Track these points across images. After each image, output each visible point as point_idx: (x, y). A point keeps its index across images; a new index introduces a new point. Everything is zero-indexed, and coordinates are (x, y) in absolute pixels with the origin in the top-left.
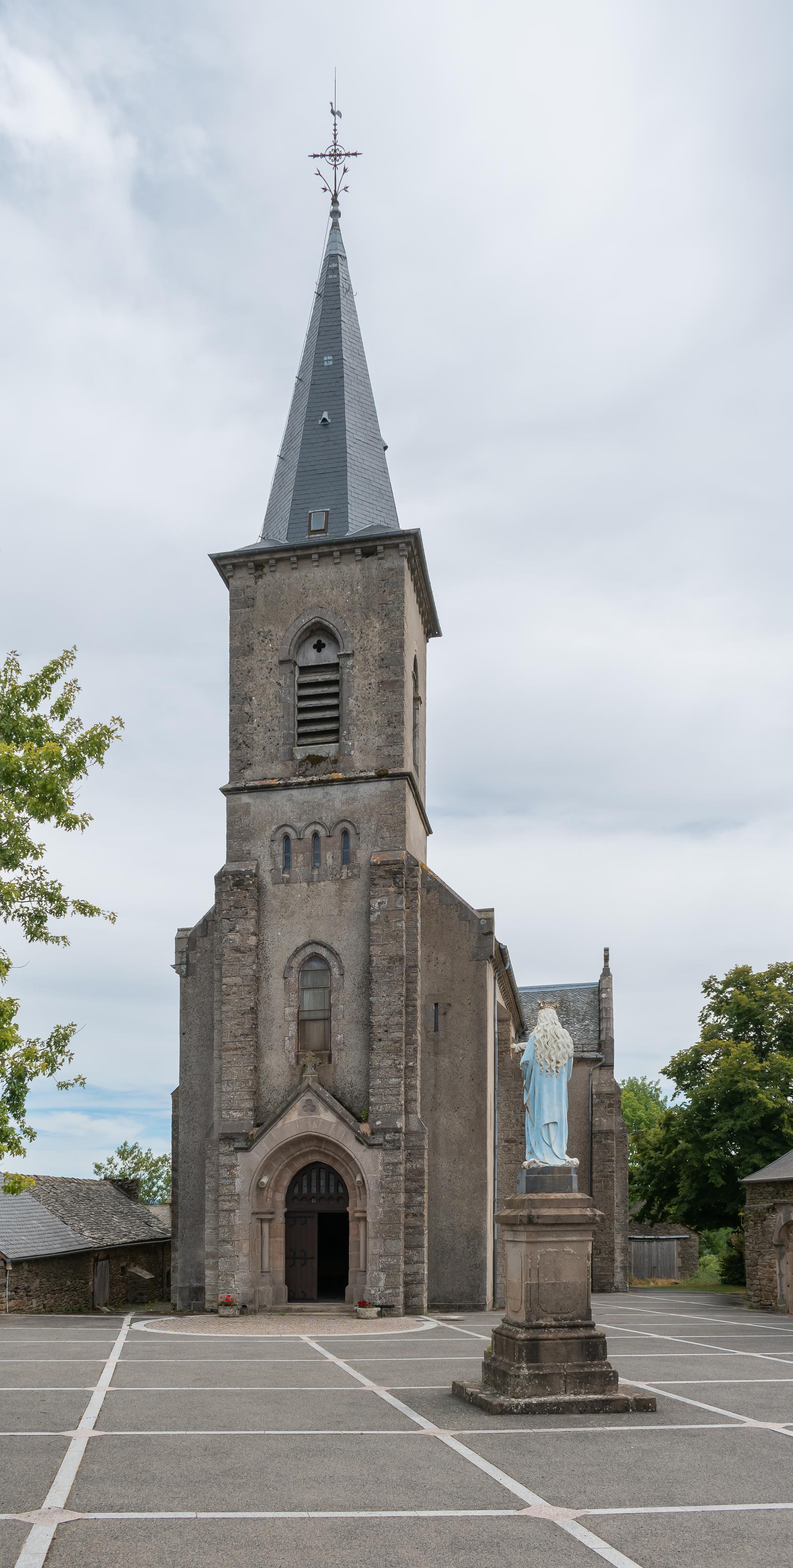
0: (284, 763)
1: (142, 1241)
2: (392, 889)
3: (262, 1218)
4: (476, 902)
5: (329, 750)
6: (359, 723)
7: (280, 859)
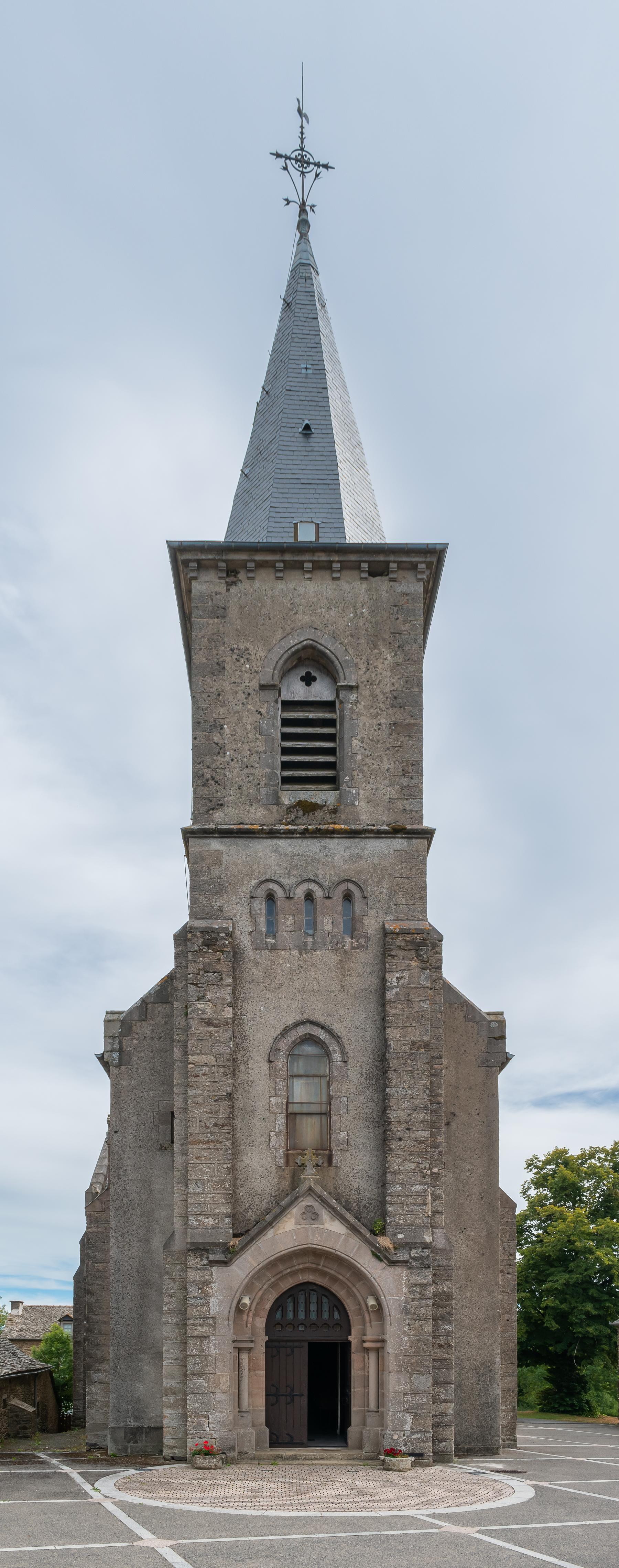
0: (266, 806)
1: (19, 1372)
4: (484, 1004)
5: (324, 796)
6: (365, 768)
7: (262, 920)
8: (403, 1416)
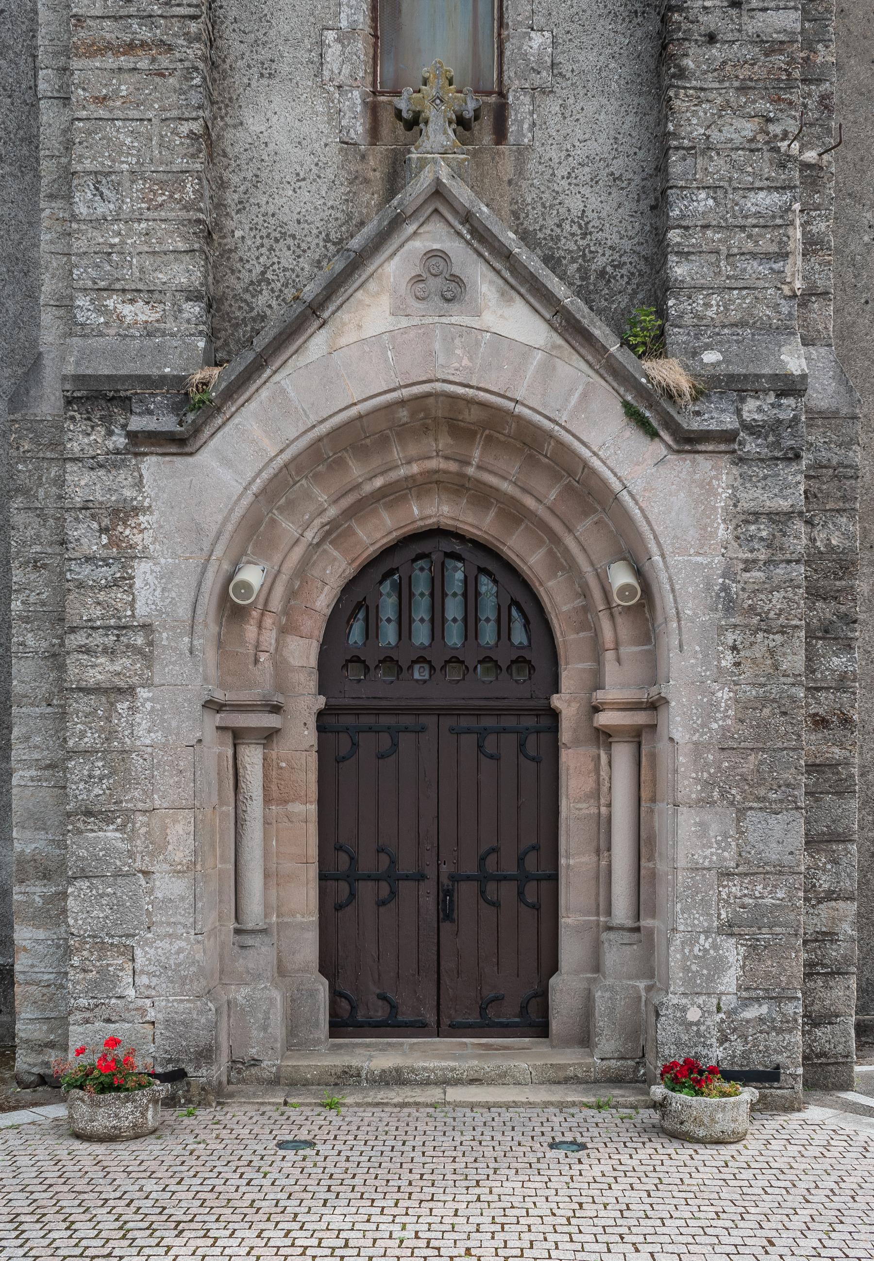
3: (240, 725)
8: (715, 946)
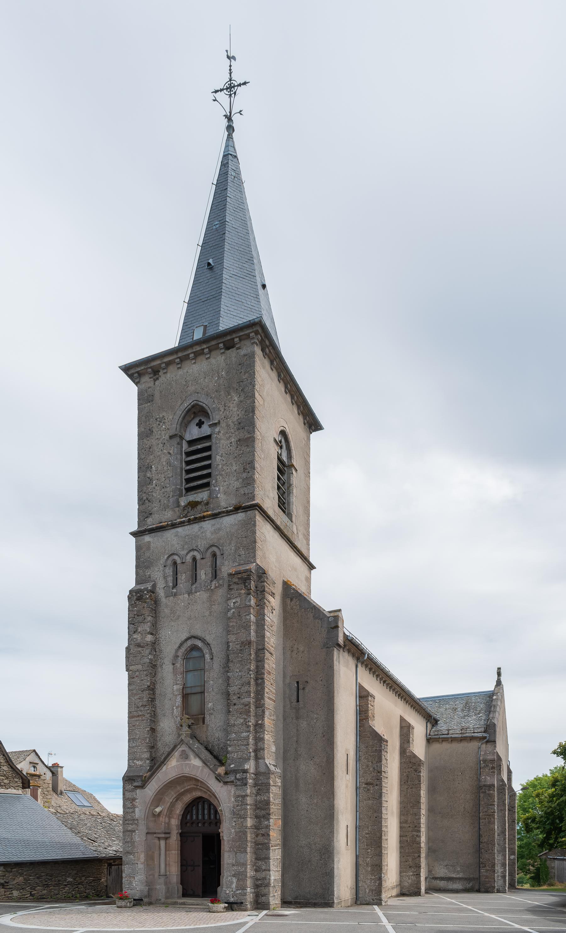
2: (243, 592)
4: (327, 606)
7: (170, 579)
